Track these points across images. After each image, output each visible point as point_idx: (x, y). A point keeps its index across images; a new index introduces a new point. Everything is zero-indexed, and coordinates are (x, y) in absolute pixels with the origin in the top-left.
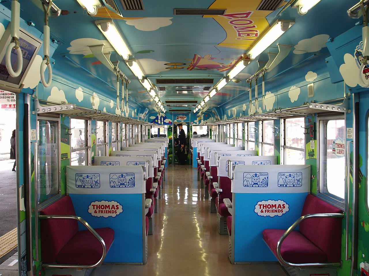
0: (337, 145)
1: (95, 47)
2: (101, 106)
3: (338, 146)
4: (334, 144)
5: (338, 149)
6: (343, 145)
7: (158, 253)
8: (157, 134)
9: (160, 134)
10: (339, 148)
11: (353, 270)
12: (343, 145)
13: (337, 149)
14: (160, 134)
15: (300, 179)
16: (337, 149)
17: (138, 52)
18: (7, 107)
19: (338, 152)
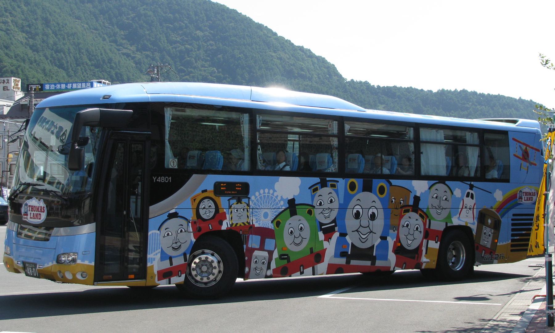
0: (30, 208)
1: (482, 189)
2: (134, 16)
3: (32, 208)
4: (26, 206)
5: (32, 212)
6: (532, 193)
7: (325, 171)
8: (83, 84)
9: (81, 84)
10: (34, 212)
11: (23, 146)
12: (532, 193)
13: (31, 213)
14: (85, 84)
15: (520, 146)
16: (31, 213)
17: (430, 188)
18: (71, 144)
19: (32, 216)
